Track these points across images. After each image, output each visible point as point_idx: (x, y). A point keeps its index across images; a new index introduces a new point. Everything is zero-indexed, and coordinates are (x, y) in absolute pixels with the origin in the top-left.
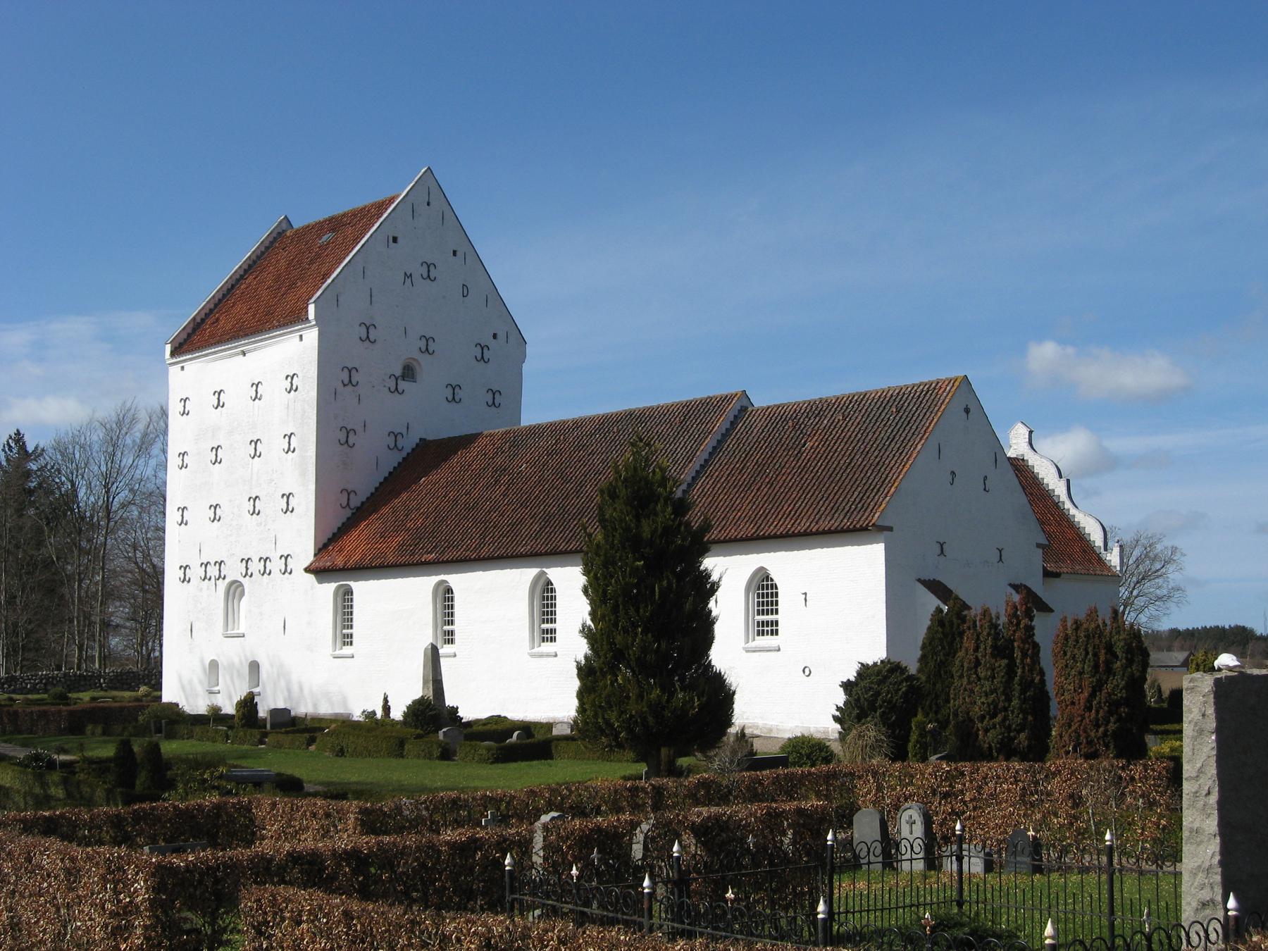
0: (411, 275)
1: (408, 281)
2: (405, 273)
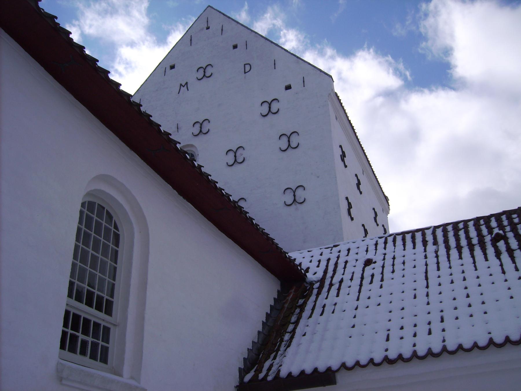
0: (187, 83)
1: (184, 89)
2: (181, 85)
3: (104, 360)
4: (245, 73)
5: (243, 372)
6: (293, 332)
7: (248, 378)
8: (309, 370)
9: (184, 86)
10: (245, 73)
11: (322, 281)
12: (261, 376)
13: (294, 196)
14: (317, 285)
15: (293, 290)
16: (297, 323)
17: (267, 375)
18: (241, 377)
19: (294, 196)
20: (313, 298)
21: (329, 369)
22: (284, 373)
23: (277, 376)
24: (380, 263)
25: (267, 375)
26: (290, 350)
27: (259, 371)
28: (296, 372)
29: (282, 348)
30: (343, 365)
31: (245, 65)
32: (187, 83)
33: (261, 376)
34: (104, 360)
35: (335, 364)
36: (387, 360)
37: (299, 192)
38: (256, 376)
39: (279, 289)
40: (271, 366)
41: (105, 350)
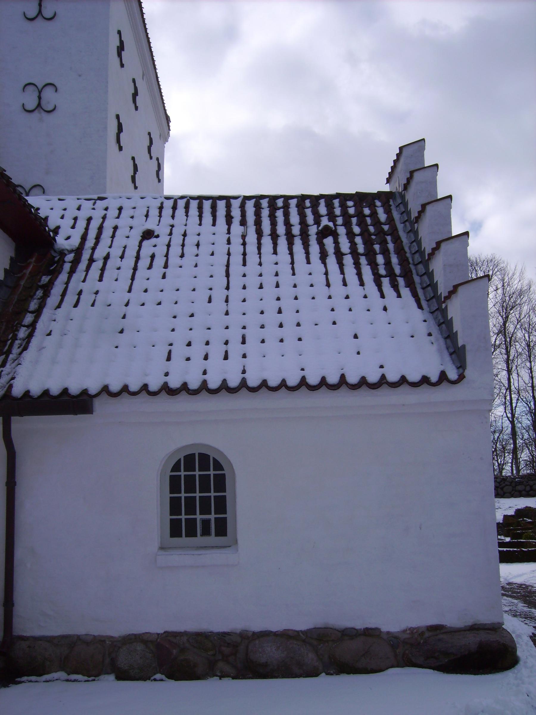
6: (33, 326)
8: (55, 390)
11: (79, 251)
13: (40, 98)
14: (70, 257)
16: (38, 313)
19: (40, 98)
20: (63, 277)
21: (85, 392)
22: (18, 391)
24: (164, 239)
26: (28, 355)
28: (36, 390)
29: (15, 350)
35: (94, 388)
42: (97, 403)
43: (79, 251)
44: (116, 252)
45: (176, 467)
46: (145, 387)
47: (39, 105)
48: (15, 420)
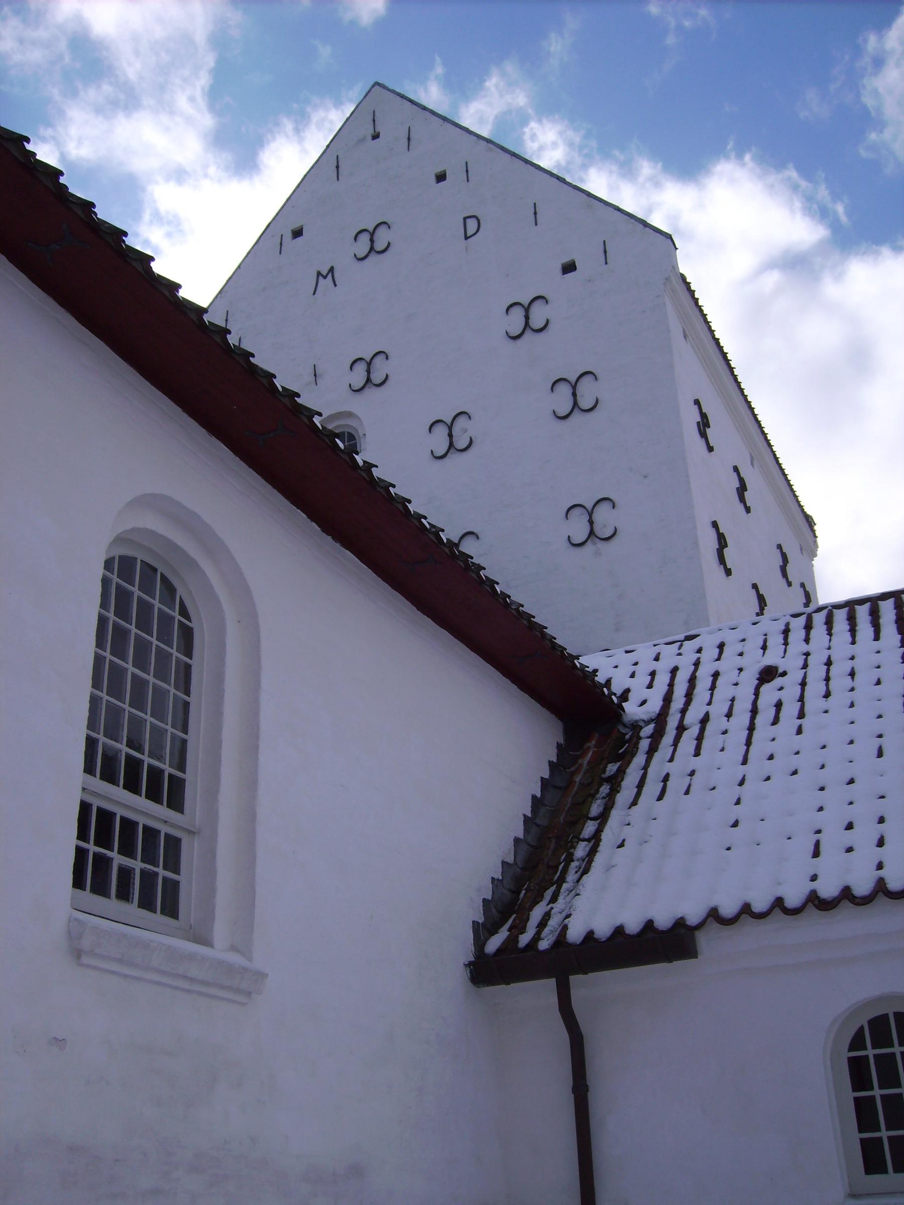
0: (332, 270)
3: (171, 909)
4: (466, 238)
5: (482, 932)
6: (596, 838)
7: (494, 944)
8: (633, 925)
9: (325, 277)
10: (466, 238)
11: (661, 719)
12: (524, 939)
14: (648, 730)
15: (593, 742)
16: (603, 818)
17: (537, 938)
18: (479, 944)
20: (639, 759)
21: (680, 923)
22: (575, 934)
23: (561, 941)
24: (795, 676)
25: (537, 938)
27: (519, 928)
28: (603, 928)
29: (571, 877)
30: (714, 914)
31: (465, 219)
32: (332, 270)
33: (524, 939)
34: (171, 909)
36: (814, 901)
37: (603, 515)
38: (512, 940)
39: (561, 741)
40: (547, 916)
41: (172, 889)
42: (703, 940)
43: (661, 719)
44: (719, 708)
45: (857, 1042)
46: (779, 902)
47: (592, 533)
48: (575, 980)
